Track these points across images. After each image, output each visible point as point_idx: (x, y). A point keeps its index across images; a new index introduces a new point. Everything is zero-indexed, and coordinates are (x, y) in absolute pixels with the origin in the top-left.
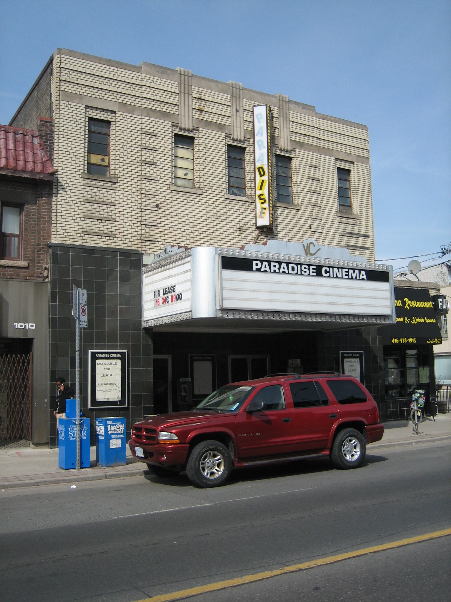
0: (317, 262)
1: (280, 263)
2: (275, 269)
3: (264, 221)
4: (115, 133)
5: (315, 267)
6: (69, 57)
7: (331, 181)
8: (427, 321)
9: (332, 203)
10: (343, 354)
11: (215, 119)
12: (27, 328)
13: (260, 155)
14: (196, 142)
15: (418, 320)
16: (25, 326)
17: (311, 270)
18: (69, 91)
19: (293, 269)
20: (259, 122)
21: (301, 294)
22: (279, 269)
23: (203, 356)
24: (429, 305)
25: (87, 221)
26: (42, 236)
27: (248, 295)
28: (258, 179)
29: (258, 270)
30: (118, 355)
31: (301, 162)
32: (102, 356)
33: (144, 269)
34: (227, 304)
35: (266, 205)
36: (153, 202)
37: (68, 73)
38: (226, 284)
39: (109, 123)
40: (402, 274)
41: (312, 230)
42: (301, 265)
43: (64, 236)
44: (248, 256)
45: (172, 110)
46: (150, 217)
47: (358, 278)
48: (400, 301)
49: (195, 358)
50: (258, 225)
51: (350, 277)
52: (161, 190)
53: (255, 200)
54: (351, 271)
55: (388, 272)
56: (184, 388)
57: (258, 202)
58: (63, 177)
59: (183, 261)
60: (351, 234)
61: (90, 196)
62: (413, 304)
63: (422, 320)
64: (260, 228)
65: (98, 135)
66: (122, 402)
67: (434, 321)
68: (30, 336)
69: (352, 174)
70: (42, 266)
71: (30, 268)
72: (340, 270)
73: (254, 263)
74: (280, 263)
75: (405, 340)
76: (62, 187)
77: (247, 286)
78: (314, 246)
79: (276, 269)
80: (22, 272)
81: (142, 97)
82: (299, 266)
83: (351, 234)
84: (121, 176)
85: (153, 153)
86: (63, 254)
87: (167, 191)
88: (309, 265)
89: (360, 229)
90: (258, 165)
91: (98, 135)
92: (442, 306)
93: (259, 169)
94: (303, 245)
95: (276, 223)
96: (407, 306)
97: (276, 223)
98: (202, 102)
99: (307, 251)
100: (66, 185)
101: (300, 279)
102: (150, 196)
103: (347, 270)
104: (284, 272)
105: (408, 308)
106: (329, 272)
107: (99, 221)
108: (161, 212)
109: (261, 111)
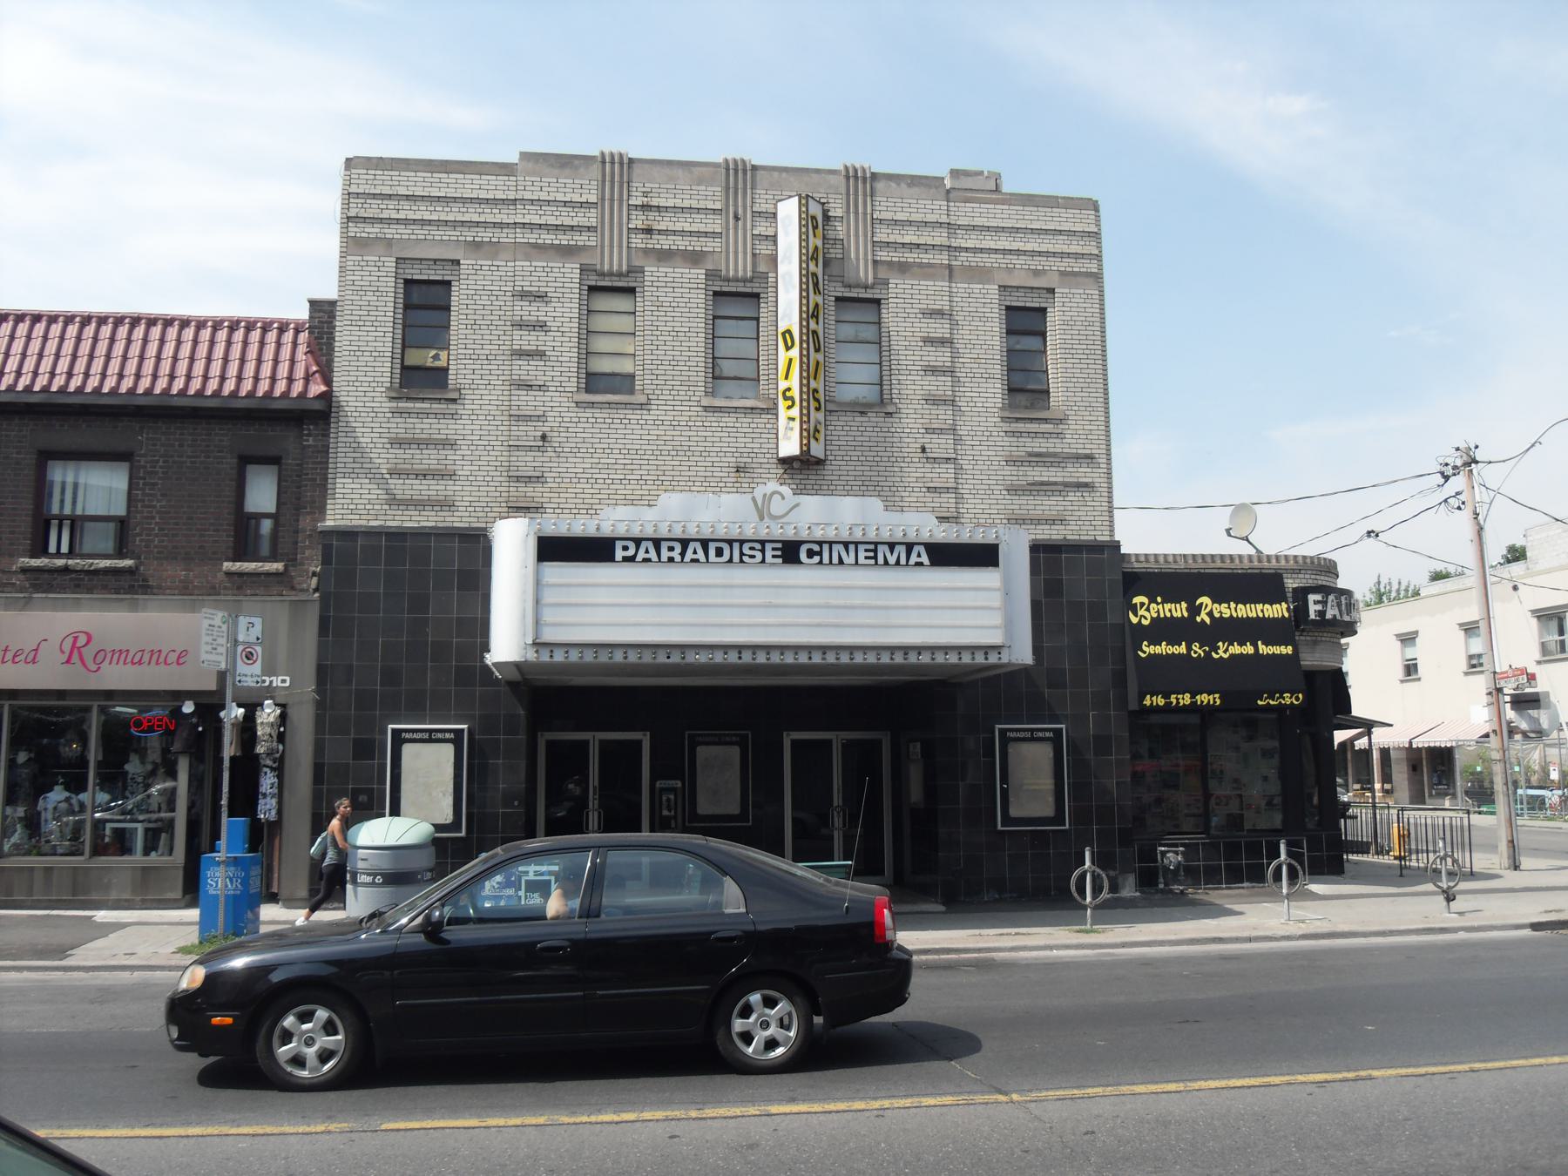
0: (790, 534)
3: (790, 446)
7: (984, 338)
10: (1003, 732)
11: (681, 243)
15: (1236, 649)
17: (769, 553)
19: (719, 552)
20: (787, 234)
22: (683, 554)
23: (1032, 730)
24: (1278, 611)
28: (783, 356)
29: (631, 559)
34: (549, 636)
35: (795, 412)
36: (532, 431)
38: (549, 597)
39: (449, 283)
40: (1369, 533)
42: (742, 542)
44: (606, 531)
45: (581, 239)
46: (527, 463)
47: (903, 561)
48: (1184, 605)
49: (1012, 735)
50: (781, 455)
51: (881, 561)
52: (558, 401)
53: (776, 404)
55: (996, 546)
56: (668, 800)
57: (782, 404)
60: (1038, 458)
62: (1225, 610)
63: (1249, 649)
64: (786, 462)
67: (1289, 650)
72: (852, 547)
73: (619, 545)
77: (602, 597)
79: (676, 554)
82: (736, 546)
83: (1038, 458)
86: (345, 546)
88: (763, 543)
89: (1073, 442)
90: (782, 328)
92: (1322, 613)
93: (783, 334)
94: (754, 499)
96: (1204, 616)
98: (652, 215)
104: (697, 561)
105: (1208, 620)
106: (820, 553)
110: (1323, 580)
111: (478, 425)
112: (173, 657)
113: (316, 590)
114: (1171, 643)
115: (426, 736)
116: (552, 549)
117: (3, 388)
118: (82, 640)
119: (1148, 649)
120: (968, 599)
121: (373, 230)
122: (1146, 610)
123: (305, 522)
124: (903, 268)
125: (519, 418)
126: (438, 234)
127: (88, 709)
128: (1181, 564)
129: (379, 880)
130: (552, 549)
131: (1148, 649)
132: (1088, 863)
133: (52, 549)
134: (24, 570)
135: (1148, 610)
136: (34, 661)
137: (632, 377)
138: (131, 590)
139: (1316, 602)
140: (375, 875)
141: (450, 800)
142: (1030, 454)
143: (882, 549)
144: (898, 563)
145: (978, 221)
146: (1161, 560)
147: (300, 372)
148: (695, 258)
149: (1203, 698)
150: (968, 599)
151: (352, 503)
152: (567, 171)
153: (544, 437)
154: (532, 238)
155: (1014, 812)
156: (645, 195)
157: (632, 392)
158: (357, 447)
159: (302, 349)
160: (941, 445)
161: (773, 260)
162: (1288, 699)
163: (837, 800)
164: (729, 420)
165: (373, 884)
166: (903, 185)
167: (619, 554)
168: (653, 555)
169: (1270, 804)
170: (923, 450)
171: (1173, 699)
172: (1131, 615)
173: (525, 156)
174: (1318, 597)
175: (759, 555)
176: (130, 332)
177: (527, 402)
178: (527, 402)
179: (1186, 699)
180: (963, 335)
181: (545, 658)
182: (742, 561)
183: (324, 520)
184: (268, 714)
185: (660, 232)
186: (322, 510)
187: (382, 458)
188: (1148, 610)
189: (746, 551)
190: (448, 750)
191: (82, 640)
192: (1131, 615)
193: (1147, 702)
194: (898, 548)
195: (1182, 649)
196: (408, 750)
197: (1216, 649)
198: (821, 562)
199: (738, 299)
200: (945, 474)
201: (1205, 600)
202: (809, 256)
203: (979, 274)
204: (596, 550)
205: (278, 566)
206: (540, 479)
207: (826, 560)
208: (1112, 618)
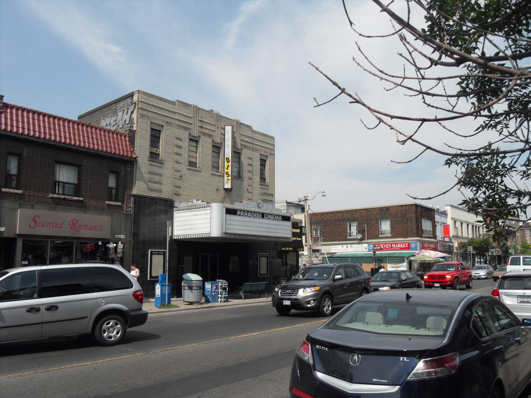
1: (248, 212)
3: (228, 186)
4: (163, 136)
8: (298, 239)
9: (257, 178)
13: (228, 151)
27: (235, 227)
28: (226, 164)
29: (240, 215)
31: (245, 155)
33: (175, 209)
34: (228, 231)
35: (230, 178)
36: (178, 174)
45: (189, 126)
46: (178, 183)
50: (225, 187)
52: (184, 167)
57: (226, 176)
59: (206, 208)
64: (226, 190)
75: (288, 249)
77: (235, 223)
89: (270, 192)
90: (226, 157)
99: (258, 207)
109: (228, 129)
111: (167, 171)
112: (99, 228)
118: (75, 222)
121: (145, 113)
123: (127, 192)
125: (176, 171)
126: (160, 117)
127: (47, 241)
133: (57, 192)
134: (51, 198)
136: (61, 227)
137: (196, 163)
138: (81, 207)
151: (139, 188)
153: (181, 176)
154: (179, 123)
155: (261, 273)
156: (201, 117)
157: (196, 167)
158: (141, 173)
164: (215, 177)
165: (197, 289)
173: (178, 101)
178: (177, 166)
180: (254, 164)
181: (228, 236)
184: (120, 245)
185: (204, 128)
186: (132, 189)
187: (147, 176)
191: (75, 222)
199: (218, 148)
203: (257, 150)
205: (120, 204)
206: (179, 187)
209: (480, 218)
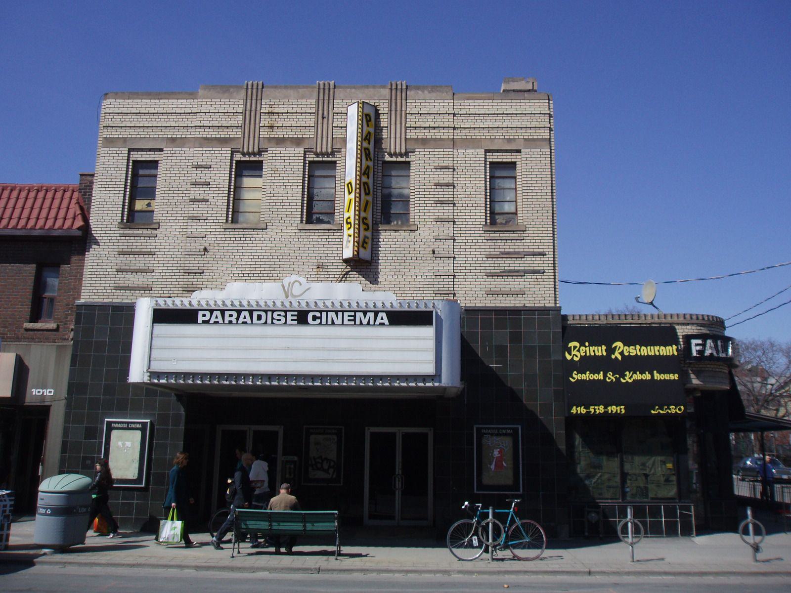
0: (304, 307)
2: (231, 319)
3: (348, 253)
5: (296, 313)
6: (114, 100)
8: (657, 376)
11: (290, 134)
12: (45, 394)
14: (265, 166)
15: (638, 376)
16: (43, 392)
18: (111, 136)
19: (259, 318)
20: (352, 125)
21: (309, 350)
22: (238, 319)
24: (670, 351)
25: (120, 275)
26: (71, 295)
28: (347, 197)
29: (206, 322)
30: (138, 426)
32: (119, 426)
34: (157, 367)
35: (351, 232)
36: (199, 245)
37: (112, 117)
41: (435, 255)
42: (273, 311)
43: (93, 294)
46: (195, 263)
47: (372, 322)
48: (604, 347)
49: (484, 431)
51: (358, 322)
54: (359, 315)
57: (346, 226)
58: (97, 230)
61: (126, 247)
62: (632, 351)
63: (647, 376)
64: (346, 261)
65: (141, 178)
66: (138, 480)
68: (47, 404)
69: (161, 170)
70: (68, 328)
71: (61, 330)
72: (340, 314)
73: (200, 313)
74: (239, 312)
76: (95, 241)
78: (301, 284)
79: (234, 319)
80: (52, 335)
81: (195, 126)
82: (270, 313)
84: (163, 221)
85: (206, 188)
87: (219, 230)
88: (286, 312)
91: (141, 178)
95: (376, 252)
97: (376, 252)
100: (100, 238)
101: (269, 330)
102: (196, 239)
103: (353, 314)
105: (620, 357)
106: (320, 318)
107: (134, 274)
108: (210, 256)
110: (716, 331)
111: (167, 245)
113: (72, 339)
114: (593, 372)
115: (126, 426)
116: (161, 316)
117: (1, 227)
119: (576, 376)
120: (413, 344)
122: (577, 351)
124: (424, 142)
128: (604, 321)
129: (49, 511)
130: (161, 316)
131: (576, 376)
132: (629, 517)
135: (579, 351)
139: (697, 345)
140: (47, 509)
141: (136, 465)
142: (502, 253)
143: (359, 315)
144: (368, 323)
145: (473, 111)
146: (700, 318)
147: (70, 215)
148: (297, 142)
149: (613, 409)
150: (413, 344)
152: (226, 95)
153: (205, 250)
155: (486, 481)
156: (271, 106)
159: (74, 201)
160: (444, 248)
161: (344, 140)
162: (673, 410)
163: (398, 470)
165: (45, 514)
166: (426, 92)
167: (200, 319)
168: (220, 319)
169: (667, 481)
170: (434, 252)
171: (592, 409)
172: (567, 354)
174: (700, 341)
175: (283, 319)
176: (54, 195)
177: (197, 228)
178: (197, 228)
179: (600, 409)
180: (460, 179)
182: (272, 323)
183: (79, 298)
188: (579, 351)
189: (275, 316)
190: (138, 434)
192: (567, 354)
193: (574, 411)
194: (369, 314)
195: (600, 376)
196: (114, 433)
197: (624, 376)
198: (320, 323)
199: (320, 167)
200: (445, 266)
201: (619, 344)
202: (365, 138)
204: (187, 316)
207: (324, 322)
208: (555, 357)
209: (214, 539)
